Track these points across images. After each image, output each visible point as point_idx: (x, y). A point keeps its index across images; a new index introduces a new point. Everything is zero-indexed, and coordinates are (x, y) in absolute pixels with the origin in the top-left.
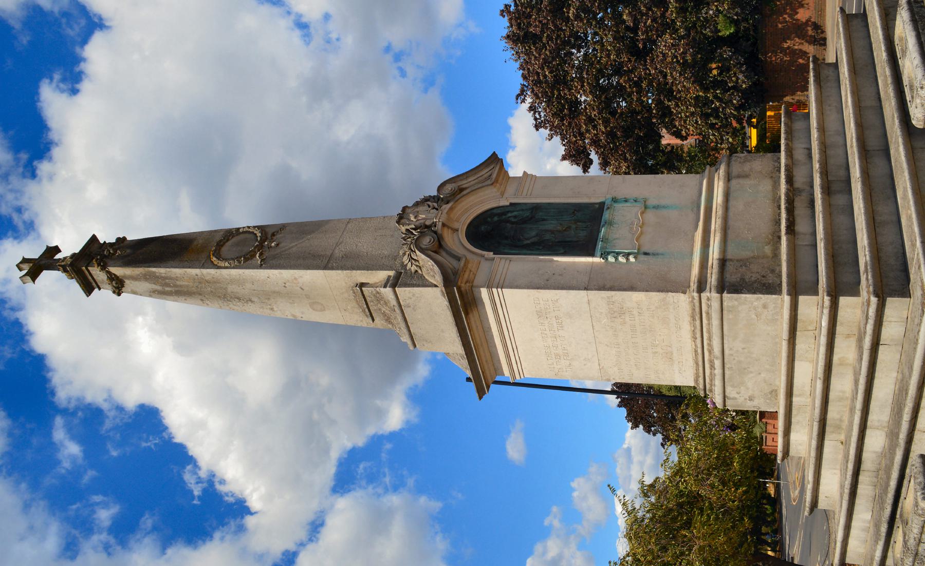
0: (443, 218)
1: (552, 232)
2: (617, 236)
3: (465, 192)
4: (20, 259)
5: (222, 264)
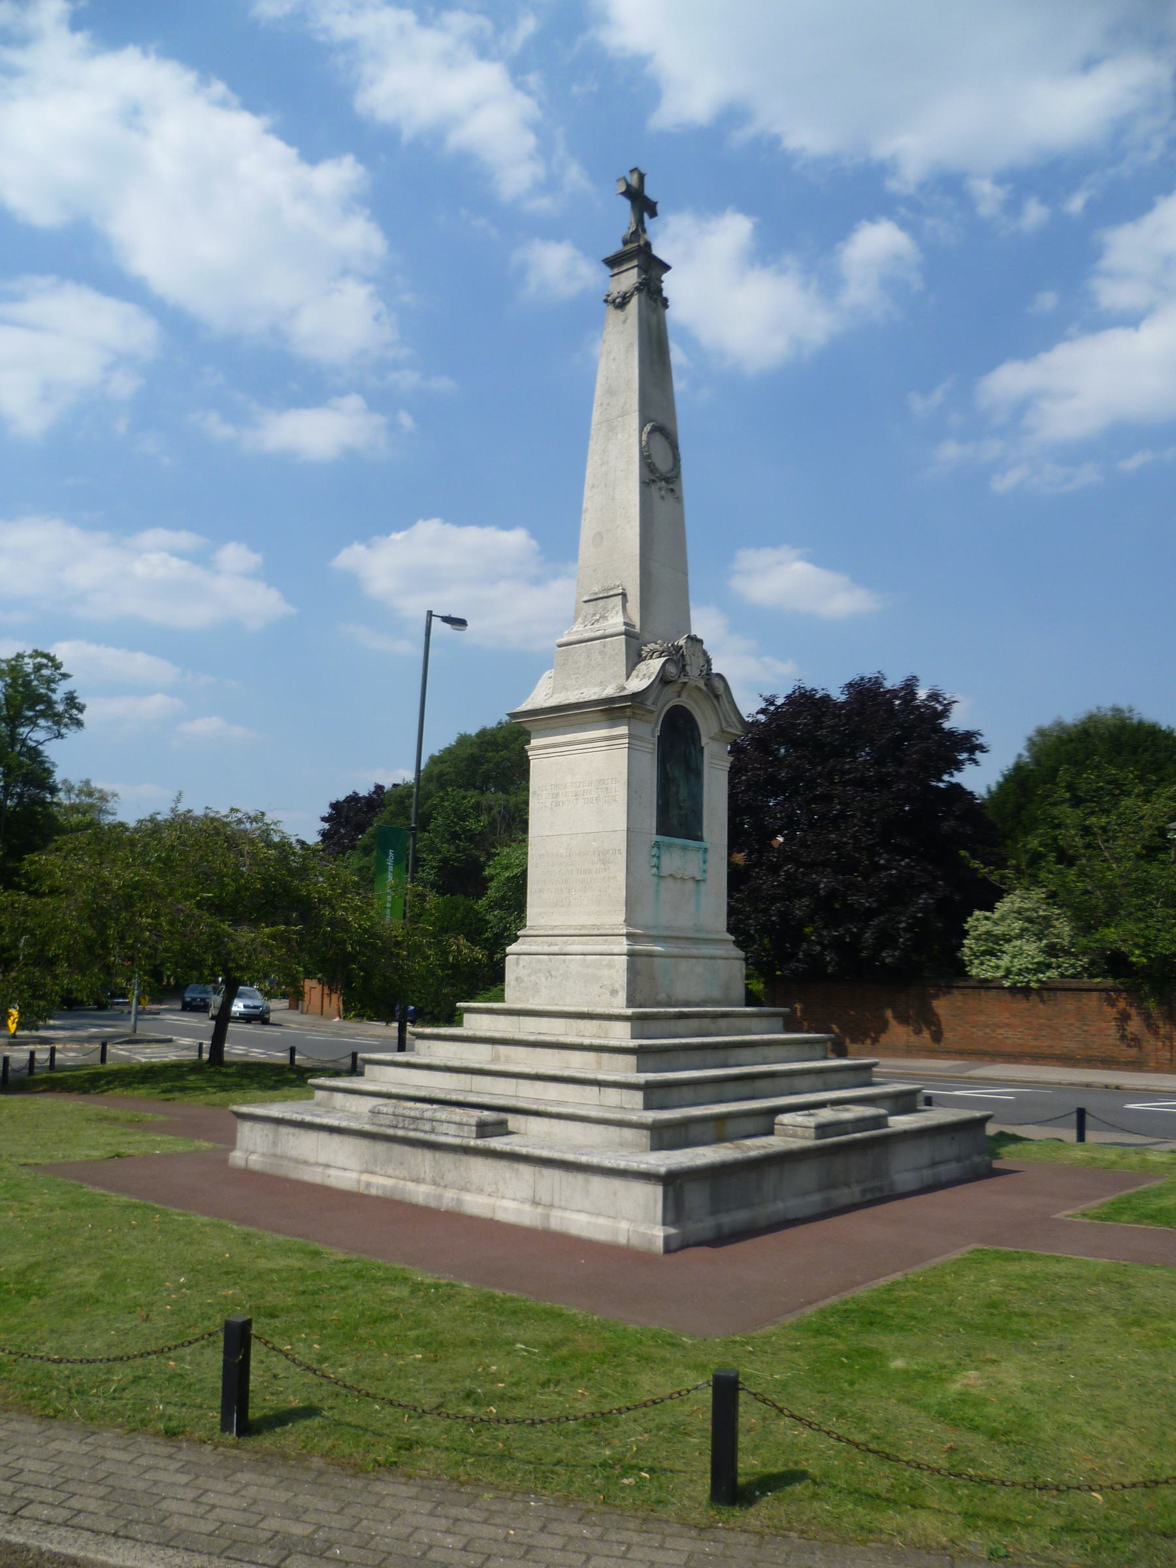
0: (692, 683)
1: (677, 793)
2: (175, 563)
3: (715, 702)
4: (643, 171)
5: (644, 437)
